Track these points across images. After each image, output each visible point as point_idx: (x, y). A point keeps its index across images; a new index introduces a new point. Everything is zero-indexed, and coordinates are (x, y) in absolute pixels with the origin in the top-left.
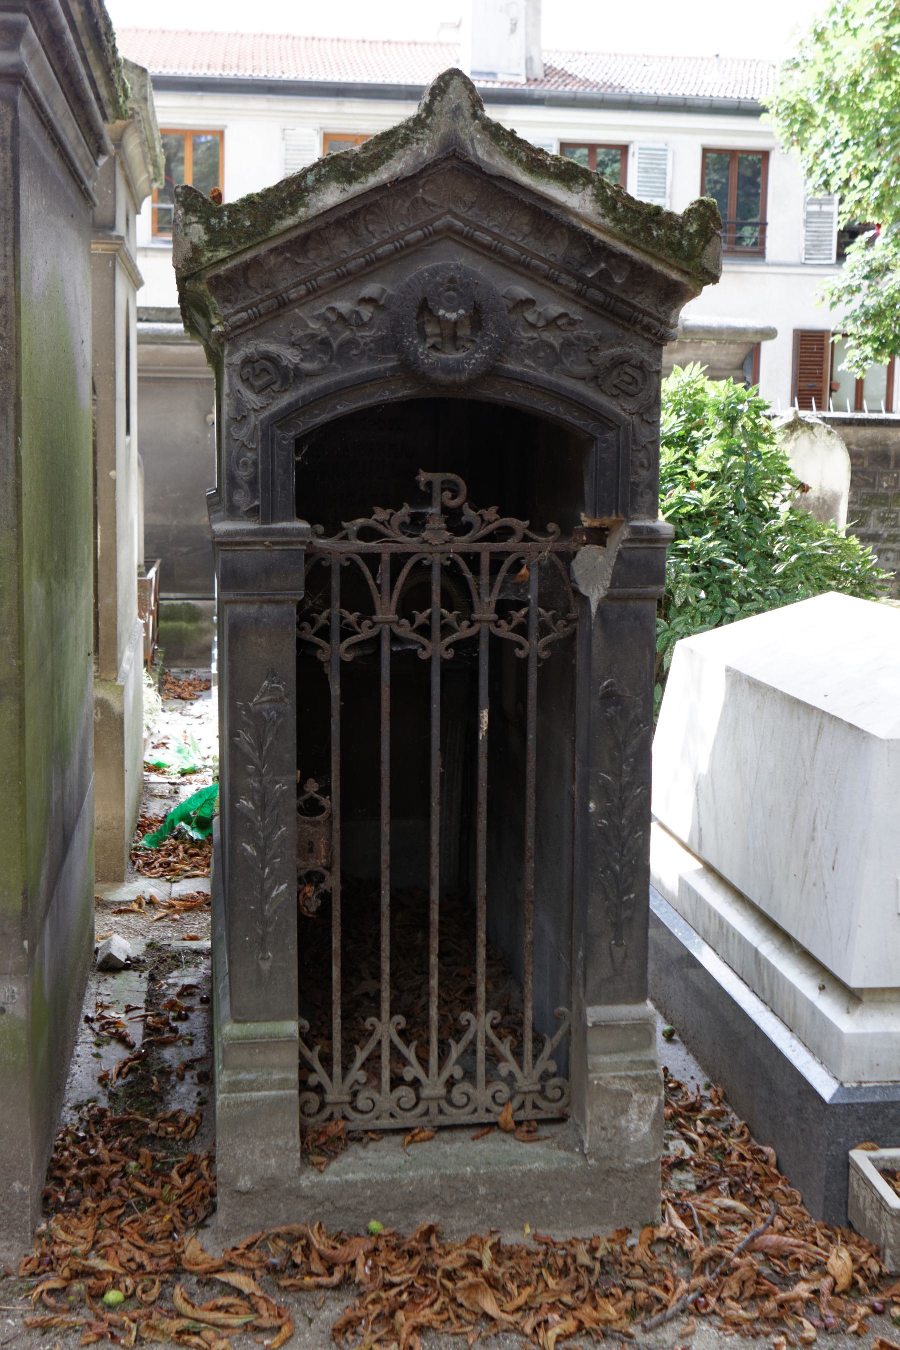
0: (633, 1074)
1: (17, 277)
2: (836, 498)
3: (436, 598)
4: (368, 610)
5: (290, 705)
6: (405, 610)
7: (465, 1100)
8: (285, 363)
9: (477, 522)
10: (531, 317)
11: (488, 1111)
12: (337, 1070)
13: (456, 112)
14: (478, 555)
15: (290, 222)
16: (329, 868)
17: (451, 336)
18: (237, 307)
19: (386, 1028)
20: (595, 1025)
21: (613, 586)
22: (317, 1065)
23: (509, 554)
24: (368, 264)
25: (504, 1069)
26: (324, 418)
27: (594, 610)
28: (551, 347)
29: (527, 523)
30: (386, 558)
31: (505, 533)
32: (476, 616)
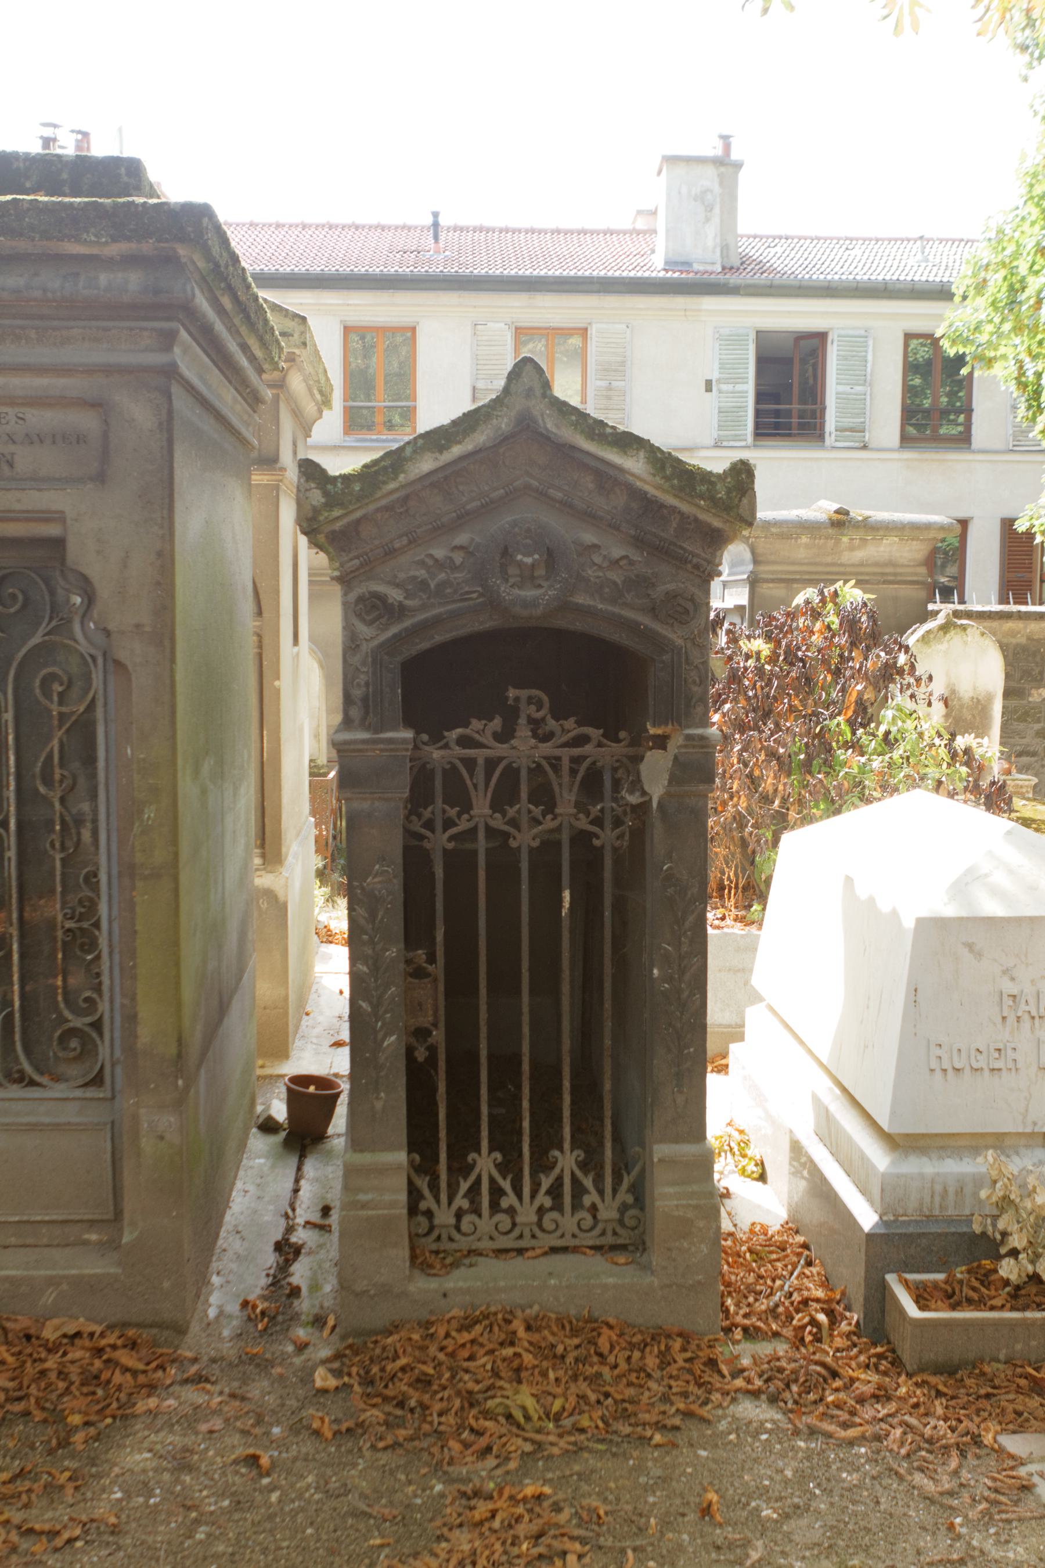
0: (693, 1202)
1: (172, 534)
2: (990, 698)
3: (524, 795)
4: (466, 807)
5: (397, 884)
6: (497, 805)
7: (553, 1227)
8: (390, 601)
9: (558, 731)
10: (597, 559)
11: (574, 1236)
12: (444, 1197)
13: (529, 393)
14: (559, 759)
15: (392, 486)
16: (435, 1025)
17: (528, 577)
18: (351, 555)
19: (485, 1163)
20: (660, 1160)
21: (670, 782)
22: (426, 1192)
23: (585, 758)
24: (459, 518)
25: (587, 1201)
26: (425, 645)
27: (655, 805)
28: (615, 583)
29: (601, 731)
30: (481, 761)
31: (581, 740)
32: (558, 811)
